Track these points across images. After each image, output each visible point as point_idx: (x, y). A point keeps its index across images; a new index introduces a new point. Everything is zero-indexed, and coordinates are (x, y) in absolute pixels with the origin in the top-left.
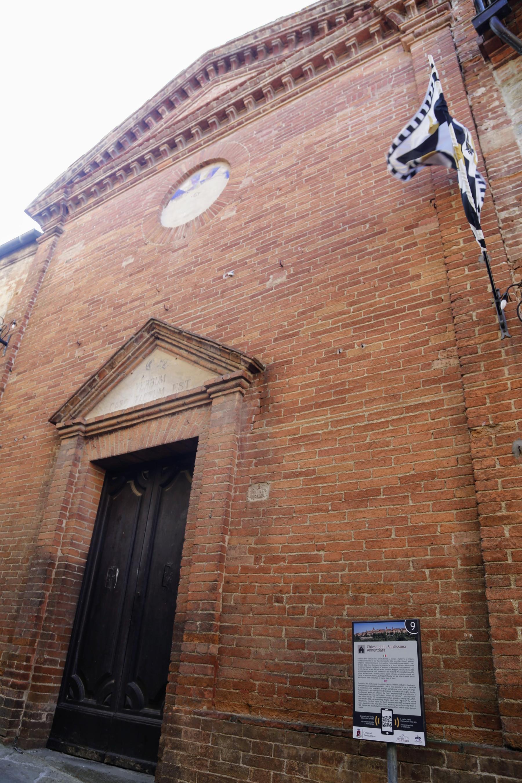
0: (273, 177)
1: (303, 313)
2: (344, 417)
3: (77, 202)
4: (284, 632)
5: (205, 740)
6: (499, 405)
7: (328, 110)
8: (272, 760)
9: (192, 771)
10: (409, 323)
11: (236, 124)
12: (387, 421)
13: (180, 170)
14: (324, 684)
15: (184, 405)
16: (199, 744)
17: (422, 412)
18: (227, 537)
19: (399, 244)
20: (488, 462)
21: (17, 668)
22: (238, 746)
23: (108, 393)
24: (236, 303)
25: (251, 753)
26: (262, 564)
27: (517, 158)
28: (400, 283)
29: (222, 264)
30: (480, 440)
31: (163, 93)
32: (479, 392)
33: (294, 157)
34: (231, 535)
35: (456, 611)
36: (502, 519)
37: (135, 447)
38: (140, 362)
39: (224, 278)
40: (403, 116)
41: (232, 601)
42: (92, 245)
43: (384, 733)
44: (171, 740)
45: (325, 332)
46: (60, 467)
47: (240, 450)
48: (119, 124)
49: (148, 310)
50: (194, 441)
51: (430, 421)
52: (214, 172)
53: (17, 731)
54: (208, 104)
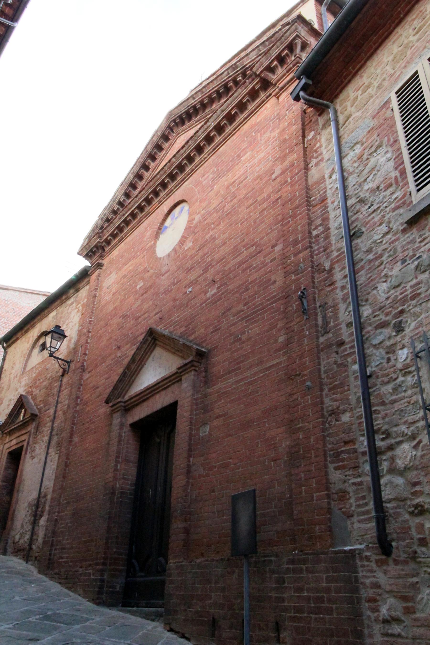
0: (210, 214)
3: (108, 242)
15: (170, 381)
18: (191, 459)
38: (149, 357)
39: (188, 293)
42: (121, 273)
52: (182, 210)
54: (170, 161)
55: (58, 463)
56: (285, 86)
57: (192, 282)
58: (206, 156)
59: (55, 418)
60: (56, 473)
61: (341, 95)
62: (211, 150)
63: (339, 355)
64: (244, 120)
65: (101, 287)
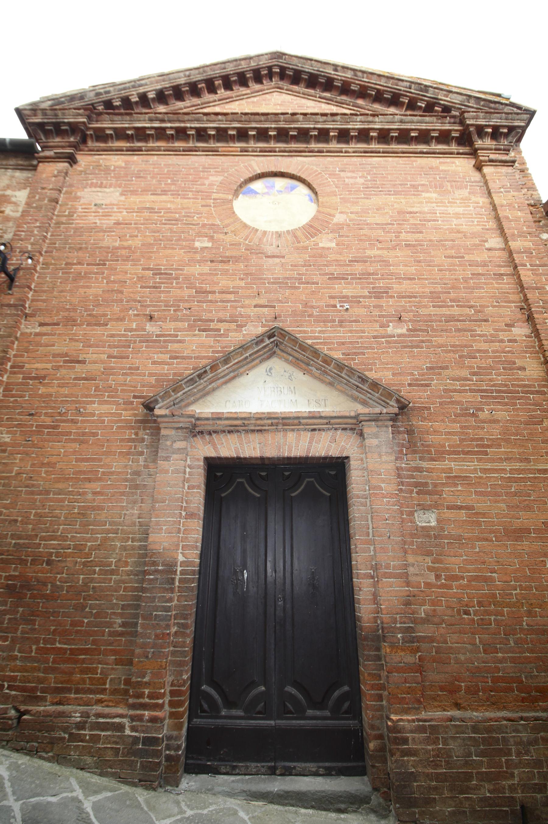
3: (101, 136)
5: (436, 741)
9: (428, 773)
11: (316, 150)
22: (469, 743)
23: (218, 387)
25: (482, 747)
26: (443, 581)
31: (223, 66)
37: (271, 452)
41: (423, 614)
44: (398, 749)
54: (294, 114)
58: (350, 150)
62: (362, 150)
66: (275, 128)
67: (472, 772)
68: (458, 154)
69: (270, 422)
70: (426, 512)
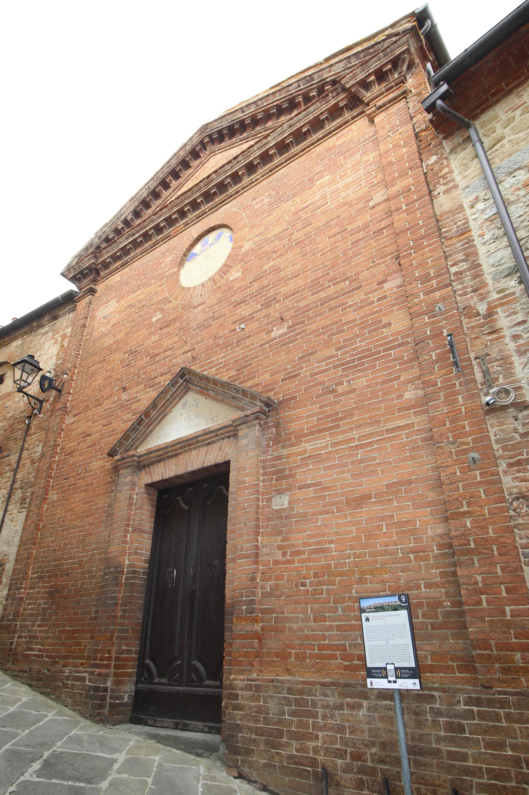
0: (269, 241)
1: (302, 358)
2: (340, 440)
3: (106, 265)
4: (309, 609)
5: (258, 700)
6: (456, 426)
7: (310, 178)
8: (310, 711)
10: (385, 363)
11: (233, 193)
12: (373, 441)
13: (191, 235)
14: (343, 648)
16: (253, 704)
17: (399, 433)
18: (260, 538)
19: (374, 297)
20: (450, 470)
21: (101, 660)
22: (283, 703)
23: (154, 429)
24: (249, 351)
25: (293, 707)
27: (464, 219)
28: (376, 330)
29: (235, 318)
30: (444, 453)
32: (440, 416)
33: (284, 223)
34: (262, 536)
35: (436, 585)
36: (464, 514)
37: (180, 471)
38: (177, 402)
40: (371, 183)
43: (390, 682)
44: (231, 703)
45: (319, 373)
46: (121, 491)
47: (263, 469)
48: (134, 194)
49: (179, 358)
50: (227, 463)
51: (405, 440)
53: (106, 711)
54: (208, 177)
55: (25, 524)
56: (385, 104)
57: (244, 318)
58: (258, 177)
59: (18, 467)
60: (21, 537)
61: (483, 116)
63: (519, 421)
64: (318, 141)
65: (93, 318)
66: (200, 195)
67: (283, 730)
68: (353, 119)
69: (179, 446)
70: (282, 496)
